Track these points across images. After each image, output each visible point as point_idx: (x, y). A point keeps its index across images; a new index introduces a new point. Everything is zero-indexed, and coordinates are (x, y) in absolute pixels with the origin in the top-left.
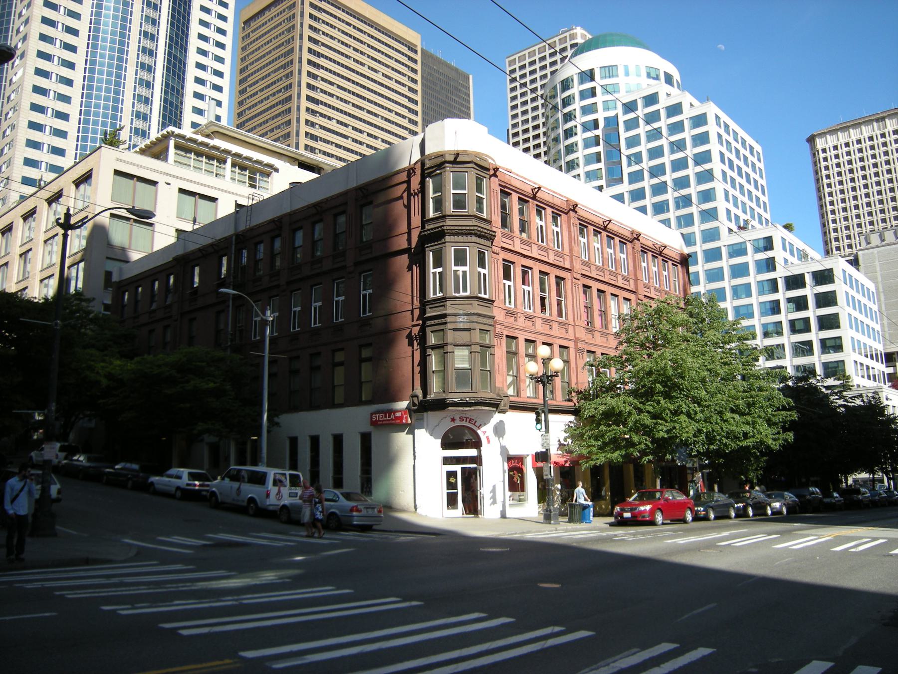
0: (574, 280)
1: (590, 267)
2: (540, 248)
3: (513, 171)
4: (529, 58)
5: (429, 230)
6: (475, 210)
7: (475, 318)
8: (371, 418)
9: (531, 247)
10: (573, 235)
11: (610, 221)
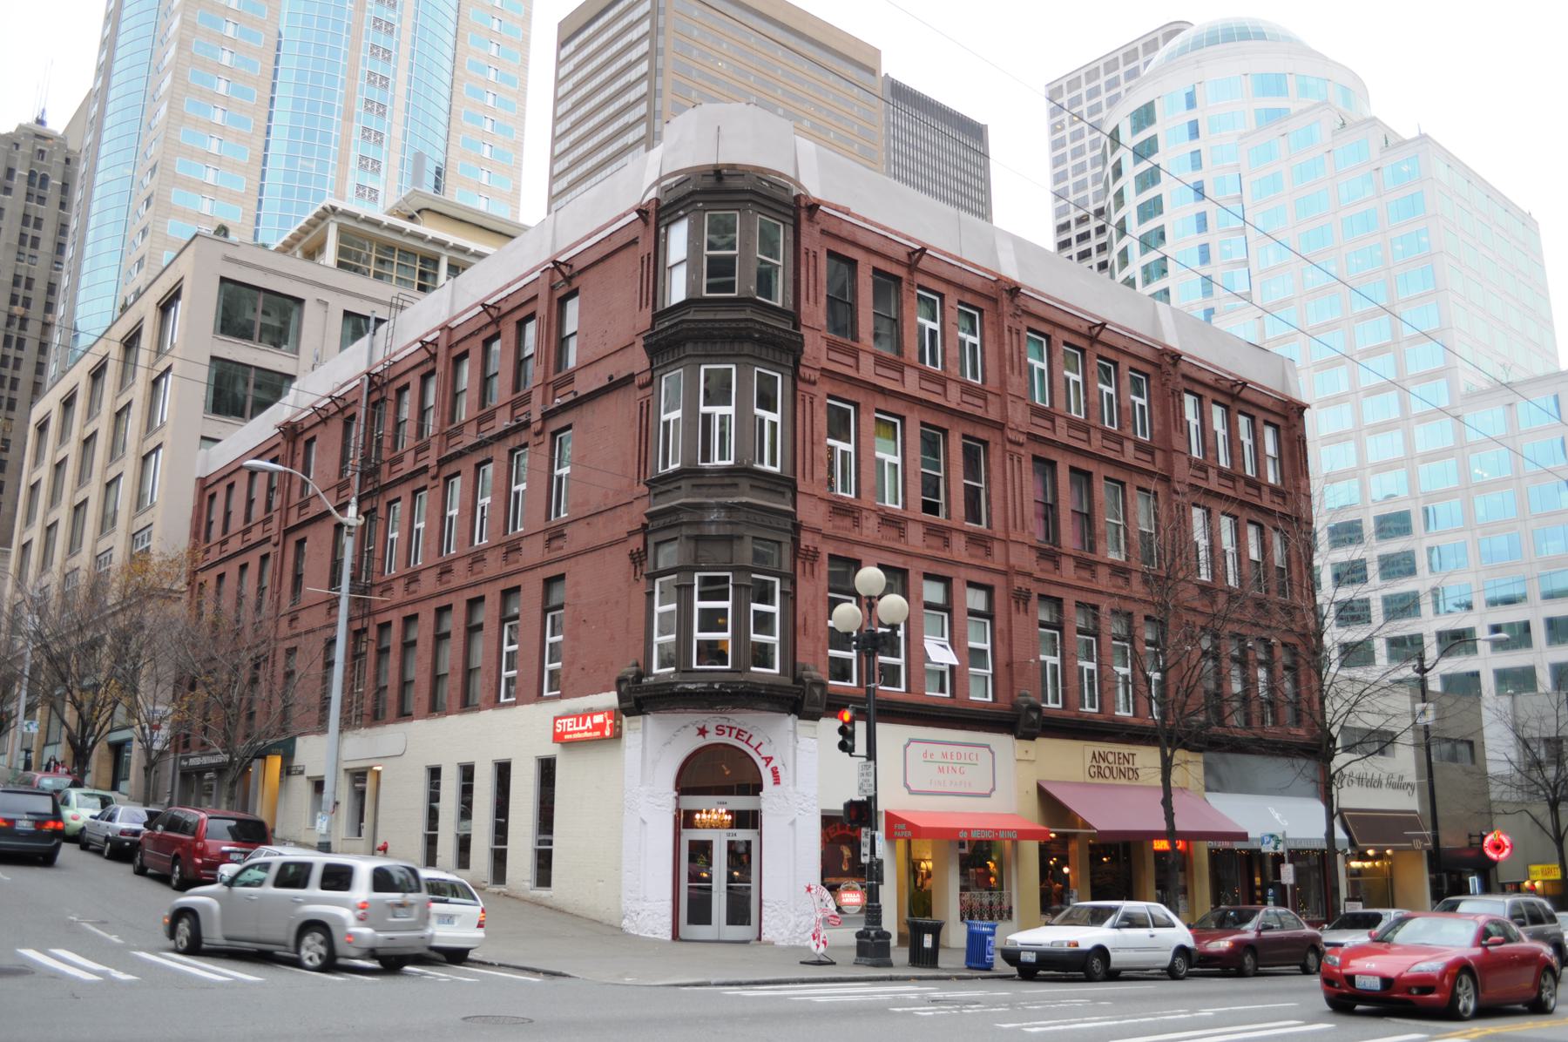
0: (1008, 446)
2: (926, 376)
3: (853, 210)
4: (1087, 83)
5: (662, 330)
6: (753, 288)
8: (555, 727)
9: (902, 373)
10: (1007, 351)
11: (1103, 325)
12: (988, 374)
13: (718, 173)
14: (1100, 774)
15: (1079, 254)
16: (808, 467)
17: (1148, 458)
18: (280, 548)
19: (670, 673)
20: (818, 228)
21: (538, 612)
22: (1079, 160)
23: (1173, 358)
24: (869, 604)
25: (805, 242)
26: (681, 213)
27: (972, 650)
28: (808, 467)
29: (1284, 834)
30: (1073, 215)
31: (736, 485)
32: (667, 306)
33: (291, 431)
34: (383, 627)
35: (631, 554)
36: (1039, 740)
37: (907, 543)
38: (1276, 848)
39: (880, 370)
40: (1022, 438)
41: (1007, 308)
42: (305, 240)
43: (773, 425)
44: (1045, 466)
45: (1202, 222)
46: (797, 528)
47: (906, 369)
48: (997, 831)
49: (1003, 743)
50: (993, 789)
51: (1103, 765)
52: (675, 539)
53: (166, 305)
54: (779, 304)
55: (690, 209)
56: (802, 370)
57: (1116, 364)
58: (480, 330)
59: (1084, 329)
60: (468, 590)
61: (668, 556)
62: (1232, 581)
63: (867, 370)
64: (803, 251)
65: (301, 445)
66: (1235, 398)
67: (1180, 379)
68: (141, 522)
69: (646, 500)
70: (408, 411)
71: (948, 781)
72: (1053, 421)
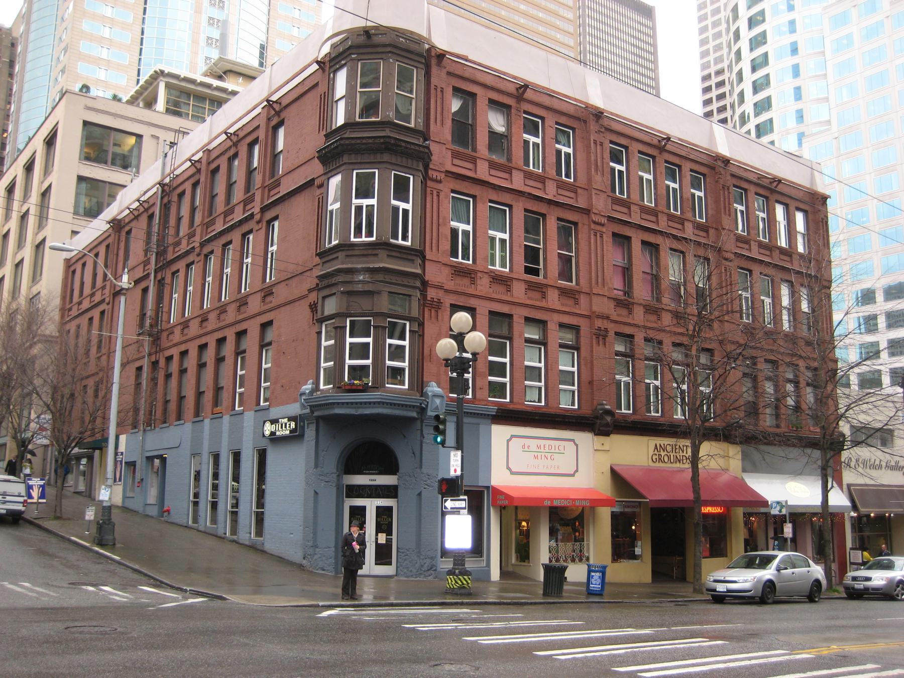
0: (593, 226)
1: (576, 193)
3: (470, 58)
4: (709, 62)
7: (380, 277)
12: (578, 174)
13: (367, 32)
14: (660, 460)
15: (717, 96)
16: (434, 241)
17: (704, 234)
18: (110, 306)
19: (329, 389)
20: (445, 71)
21: (256, 348)
22: (717, 30)
23: (723, 162)
24: (459, 338)
25: (434, 81)
26: (343, 62)
27: (527, 367)
28: (434, 241)
29: (786, 502)
30: (712, 70)
31: (376, 255)
32: (334, 128)
33: (117, 225)
34: (169, 359)
35: (310, 306)
36: (613, 436)
37: (512, 296)
38: (780, 511)
39: (493, 172)
40: (604, 220)
41: (593, 126)
42: (146, 94)
43: (406, 212)
44: (623, 240)
45: (796, 71)
46: (425, 284)
47: (514, 171)
48: (574, 500)
49: (585, 439)
50: (577, 471)
51: (663, 454)
52: (334, 294)
53: (50, 142)
54: (412, 125)
55: (348, 59)
56: (430, 172)
57: (679, 167)
58: (226, 151)
59: (655, 142)
60: (217, 333)
61: (331, 307)
62: (786, 326)
63: (483, 171)
64: (432, 87)
65: (123, 234)
66: (773, 191)
67: (729, 177)
68: (35, 290)
69: (319, 267)
70: (185, 211)
71: (541, 465)
72: (629, 208)
